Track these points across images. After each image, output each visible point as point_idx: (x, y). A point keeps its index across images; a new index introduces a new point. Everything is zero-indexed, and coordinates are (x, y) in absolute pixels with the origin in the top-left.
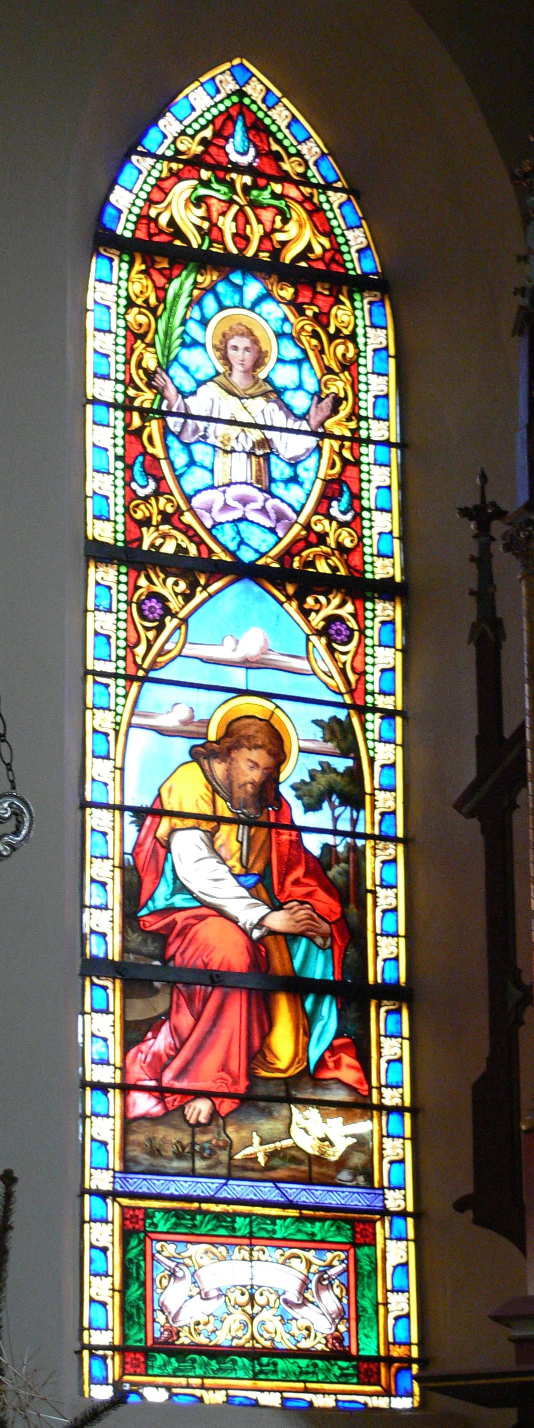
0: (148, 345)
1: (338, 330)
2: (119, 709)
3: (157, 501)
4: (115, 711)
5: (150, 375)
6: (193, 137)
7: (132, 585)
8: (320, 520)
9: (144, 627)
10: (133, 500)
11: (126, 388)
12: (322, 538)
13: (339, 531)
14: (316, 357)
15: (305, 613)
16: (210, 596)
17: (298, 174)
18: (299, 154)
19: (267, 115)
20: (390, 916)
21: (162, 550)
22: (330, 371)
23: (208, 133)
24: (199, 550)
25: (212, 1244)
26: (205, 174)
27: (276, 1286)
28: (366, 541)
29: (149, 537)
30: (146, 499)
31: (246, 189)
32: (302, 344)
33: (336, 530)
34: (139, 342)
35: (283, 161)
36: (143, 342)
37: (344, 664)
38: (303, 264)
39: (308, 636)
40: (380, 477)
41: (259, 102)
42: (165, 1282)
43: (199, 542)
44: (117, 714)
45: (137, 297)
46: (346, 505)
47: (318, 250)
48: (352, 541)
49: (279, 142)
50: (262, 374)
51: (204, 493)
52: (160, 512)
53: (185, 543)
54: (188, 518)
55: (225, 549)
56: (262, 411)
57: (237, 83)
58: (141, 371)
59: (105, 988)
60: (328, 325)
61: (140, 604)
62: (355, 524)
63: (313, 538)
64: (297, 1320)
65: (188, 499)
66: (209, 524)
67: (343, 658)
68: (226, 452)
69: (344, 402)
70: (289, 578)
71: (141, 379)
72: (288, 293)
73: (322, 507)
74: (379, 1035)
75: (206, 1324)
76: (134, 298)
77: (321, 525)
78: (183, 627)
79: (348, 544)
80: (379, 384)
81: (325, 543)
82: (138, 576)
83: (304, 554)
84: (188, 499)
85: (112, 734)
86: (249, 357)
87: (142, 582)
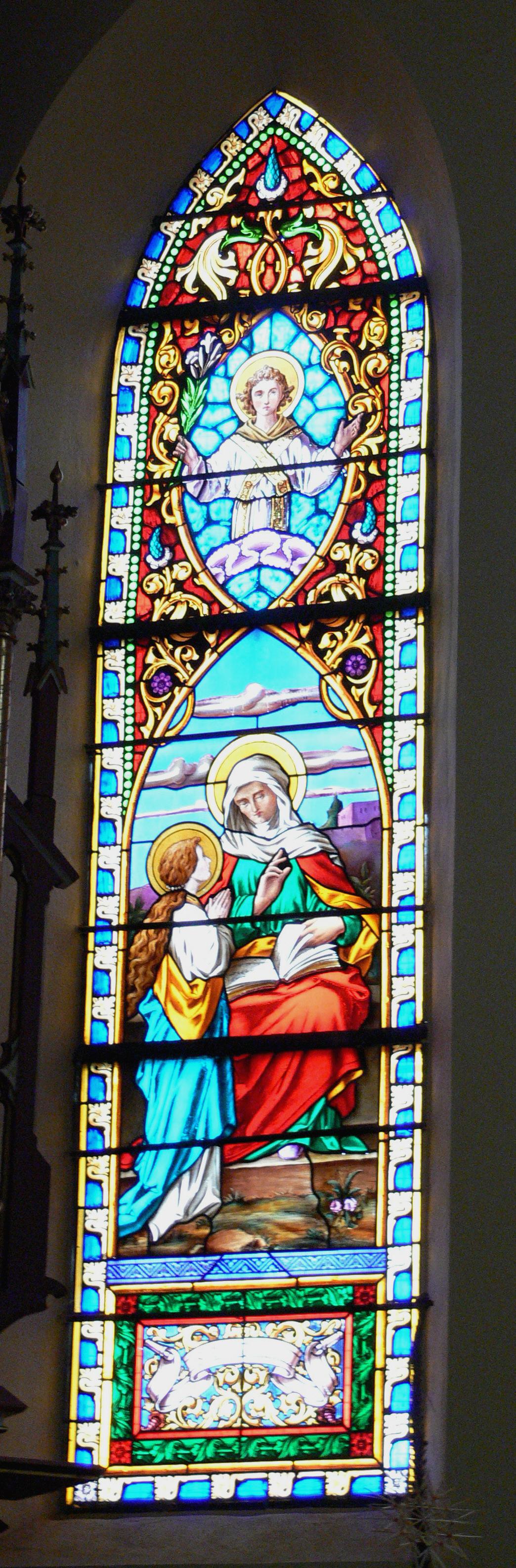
0: (171, 416)
1: (370, 345)
2: (127, 794)
3: (171, 569)
4: (122, 795)
5: (170, 446)
6: (223, 186)
7: (140, 664)
8: (341, 547)
9: (151, 703)
10: (147, 575)
11: (146, 464)
12: (341, 566)
13: (361, 554)
14: (345, 380)
15: (321, 654)
16: (221, 655)
17: (332, 191)
18: (334, 170)
19: (300, 139)
20: (409, 698)
21: (173, 618)
22: (358, 389)
23: (240, 179)
24: (210, 610)
25: (205, 1325)
26: (235, 221)
27: (266, 1362)
28: (389, 559)
29: (160, 607)
30: (160, 571)
31: (277, 224)
32: (331, 370)
33: (357, 555)
34: (161, 414)
35: (316, 180)
36: (165, 413)
37: (361, 697)
38: (335, 285)
39: (322, 677)
40: (408, 486)
41: (293, 129)
42: (154, 1368)
43: (211, 601)
44: (124, 799)
45: (163, 368)
46: (368, 526)
47: (351, 263)
48: (373, 562)
49: (313, 164)
50: (286, 412)
51: (220, 550)
52: (174, 581)
53: (197, 604)
54: (203, 579)
55: (235, 601)
56: (287, 450)
57: (271, 116)
58: (162, 444)
59: (104, 1077)
60: (359, 341)
61: (148, 683)
62: (378, 546)
63: (331, 567)
64: (287, 1395)
65: (203, 560)
66: (221, 580)
67: (360, 691)
68: (246, 502)
69: (373, 417)
70: (304, 618)
71: (161, 453)
72: (318, 320)
73: (345, 536)
74: (391, 977)
75: (193, 1407)
76: (160, 370)
77: (342, 552)
78: (190, 697)
79: (369, 566)
80: (413, 390)
81: (344, 571)
82: (146, 655)
83: (319, 587)
84: (203, 560)
85: (120, 820)
86: (275, 398)
87: (151, 658)
